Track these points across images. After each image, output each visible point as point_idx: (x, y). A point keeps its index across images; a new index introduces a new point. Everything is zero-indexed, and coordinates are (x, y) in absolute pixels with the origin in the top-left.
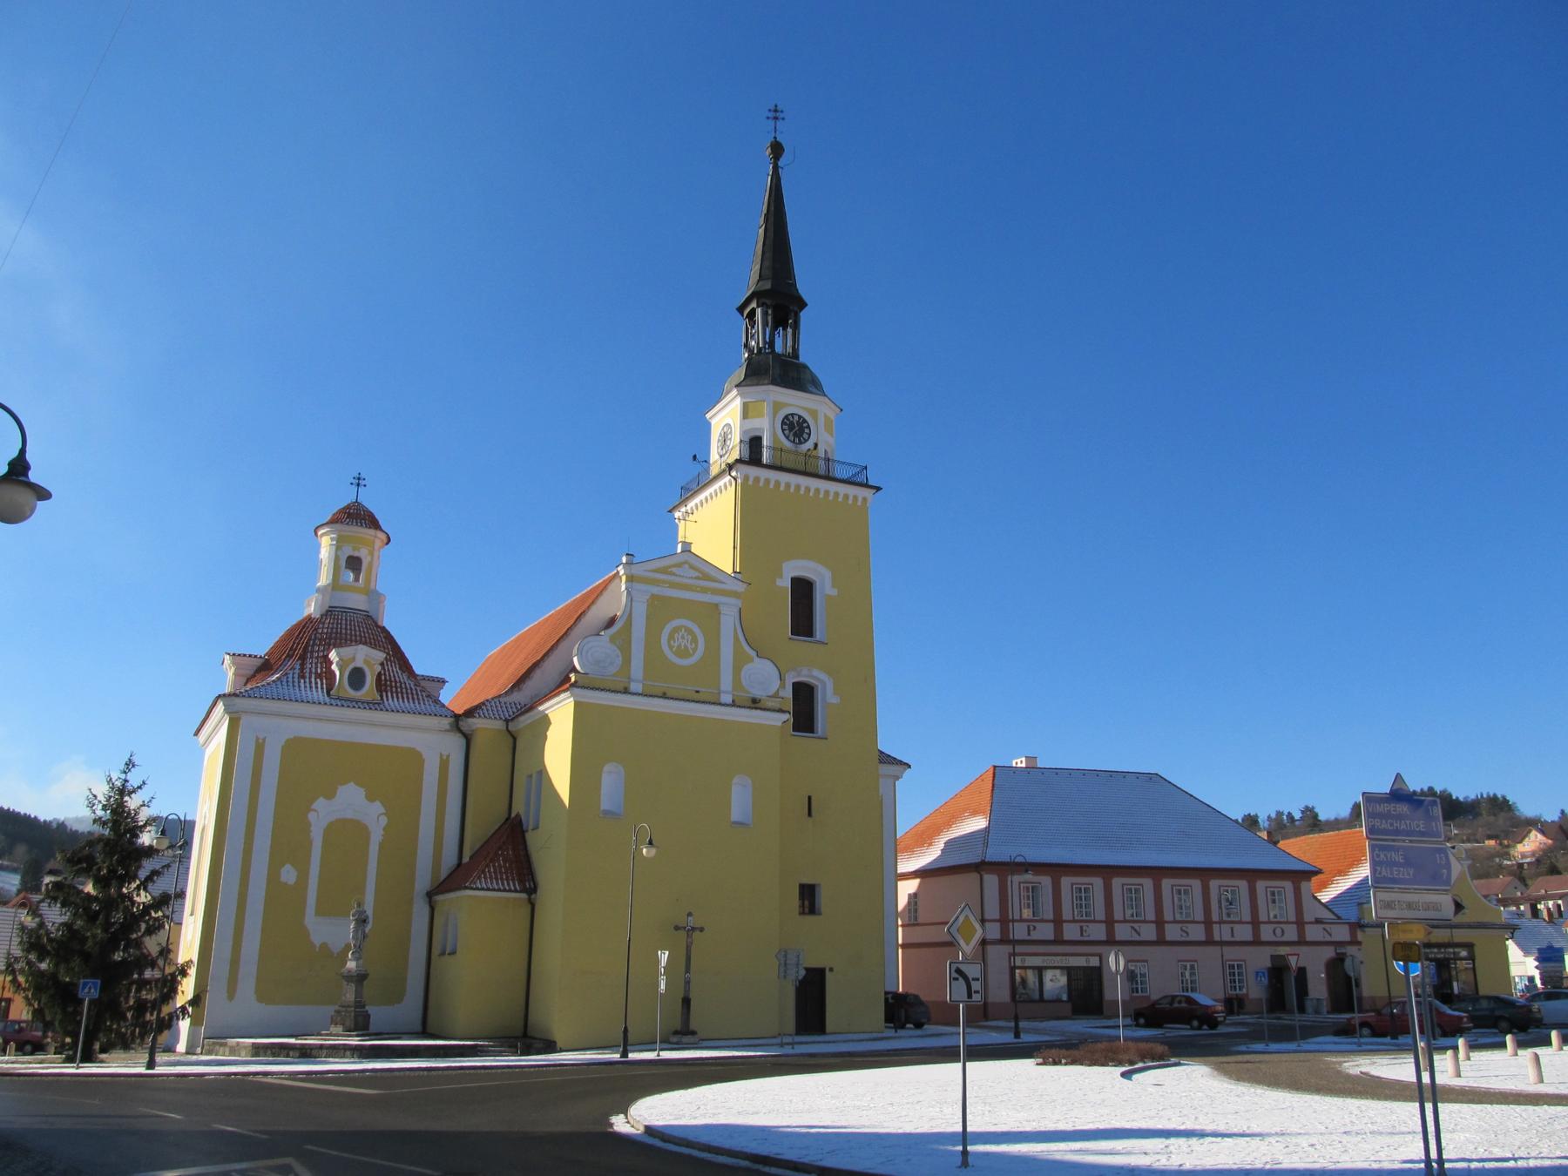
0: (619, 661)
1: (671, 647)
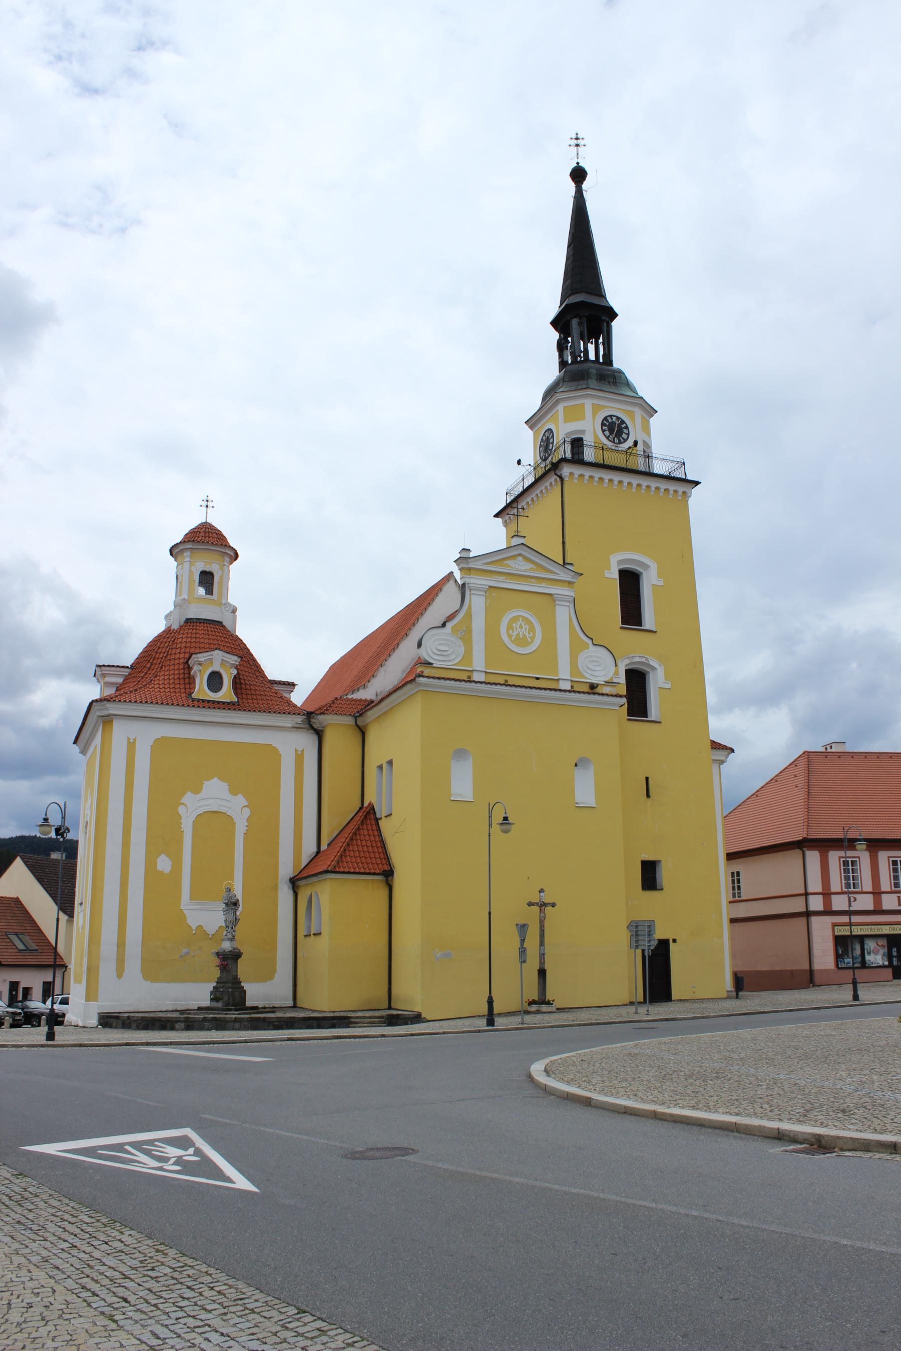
0: (462, 650)
1: (510, 636)
